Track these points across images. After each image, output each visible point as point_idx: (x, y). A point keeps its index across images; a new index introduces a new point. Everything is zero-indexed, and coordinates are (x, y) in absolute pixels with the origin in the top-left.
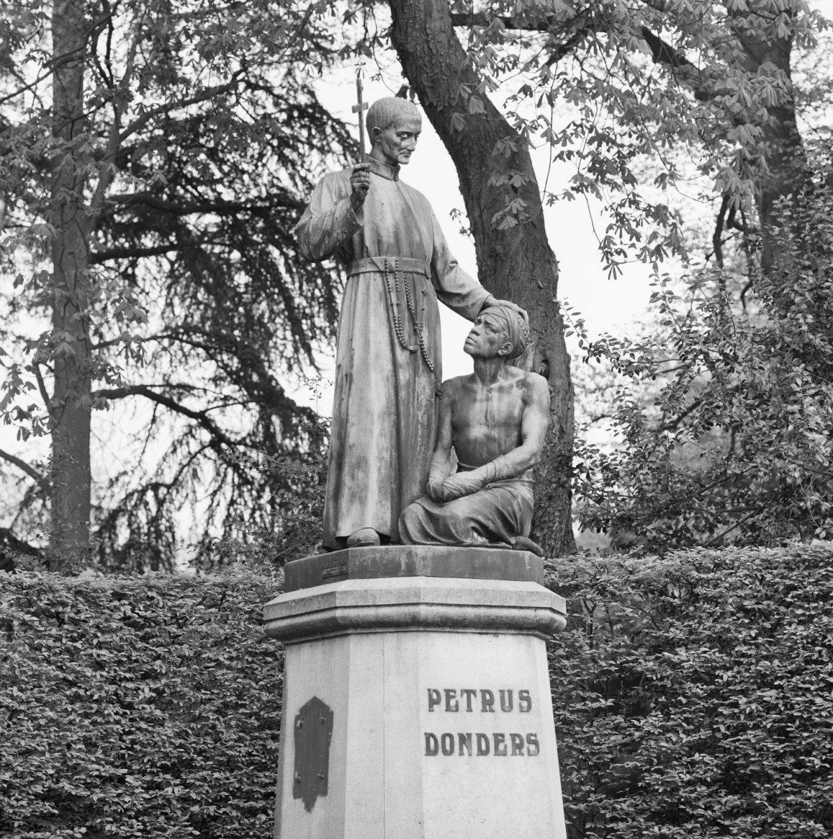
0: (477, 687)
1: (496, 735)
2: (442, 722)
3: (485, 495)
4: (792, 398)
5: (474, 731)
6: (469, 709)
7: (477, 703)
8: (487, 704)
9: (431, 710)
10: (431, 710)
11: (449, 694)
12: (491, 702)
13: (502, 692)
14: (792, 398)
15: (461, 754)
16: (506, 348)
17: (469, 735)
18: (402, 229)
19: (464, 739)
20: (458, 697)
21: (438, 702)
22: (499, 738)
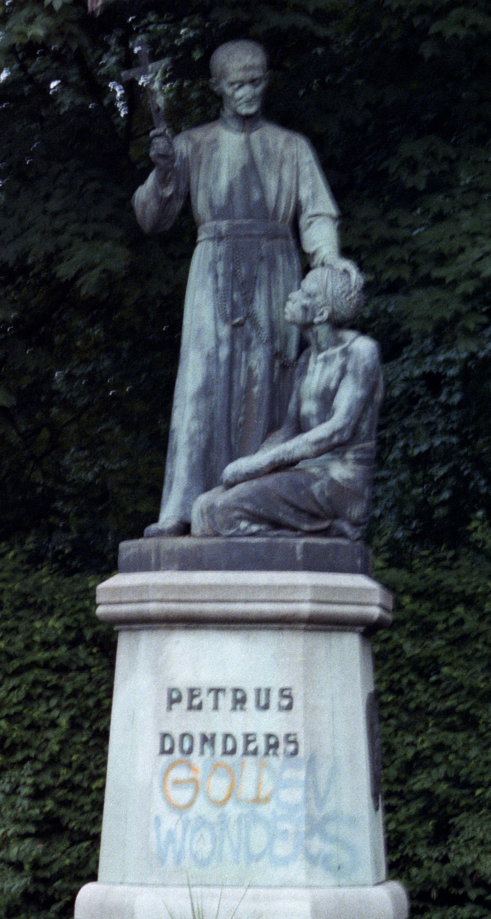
0: (229, 685)
1: (247, 736)
2: (180, 721)
3: (255, 483)
4: (334, 274)
5: (220, 730)
6: (216, 707)
7: (226, 701)
8: (240, 701)
9: (170, 709)
10: (170, 709)
11: (193, 693)
12: (243, 700)
13: (258, 691)
14: (334, 274)
15: (202, 753)
16: (346, 272)
17: (213, 736)
18: (238, 188)
19: (208, 740)
20: (203, 696)
21: (179, 700)
22: (248, 739)
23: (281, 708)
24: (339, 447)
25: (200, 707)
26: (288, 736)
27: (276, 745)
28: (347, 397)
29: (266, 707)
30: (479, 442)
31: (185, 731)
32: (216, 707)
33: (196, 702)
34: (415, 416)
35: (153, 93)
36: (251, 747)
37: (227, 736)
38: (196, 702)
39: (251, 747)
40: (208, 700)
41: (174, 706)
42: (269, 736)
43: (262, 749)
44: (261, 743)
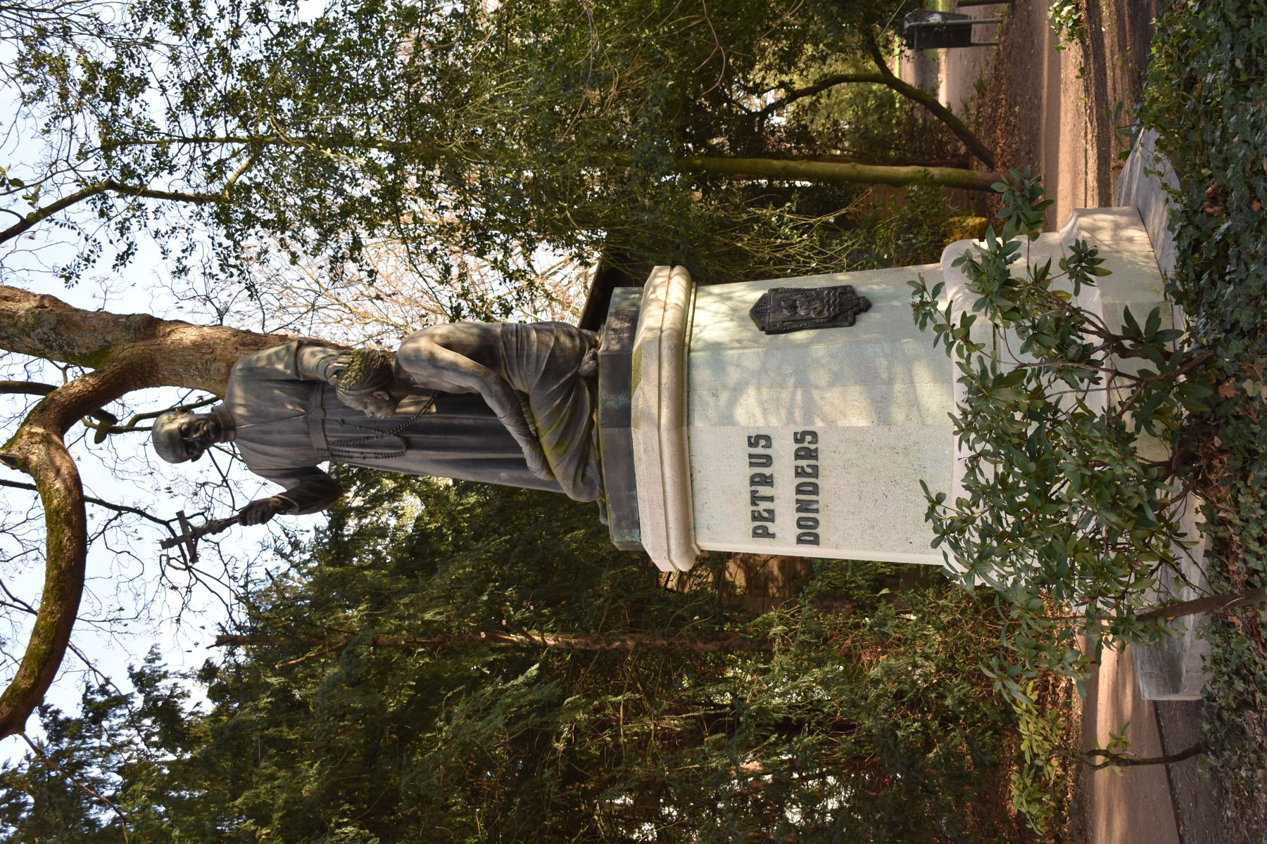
1: (798, 474)
6: (771, 499)
7: (764, 491)
8: (767, 481)
9: (773, 536)
10: (773, 536)
11: (756, 517)
13: (751, 464)
22: (799, 473)
23: (769, 446)
24: (1108, 185)
25: (771, 512)
26: (797, 441)
28: (585, 232)
30: (396, 348)
32: (771, 499)
35: (861, 47)
37: (798, 491)
38: (765, 515)
40: (763, 505)
42: (797, 457)
43: (812, 462)
44: (803, 463)
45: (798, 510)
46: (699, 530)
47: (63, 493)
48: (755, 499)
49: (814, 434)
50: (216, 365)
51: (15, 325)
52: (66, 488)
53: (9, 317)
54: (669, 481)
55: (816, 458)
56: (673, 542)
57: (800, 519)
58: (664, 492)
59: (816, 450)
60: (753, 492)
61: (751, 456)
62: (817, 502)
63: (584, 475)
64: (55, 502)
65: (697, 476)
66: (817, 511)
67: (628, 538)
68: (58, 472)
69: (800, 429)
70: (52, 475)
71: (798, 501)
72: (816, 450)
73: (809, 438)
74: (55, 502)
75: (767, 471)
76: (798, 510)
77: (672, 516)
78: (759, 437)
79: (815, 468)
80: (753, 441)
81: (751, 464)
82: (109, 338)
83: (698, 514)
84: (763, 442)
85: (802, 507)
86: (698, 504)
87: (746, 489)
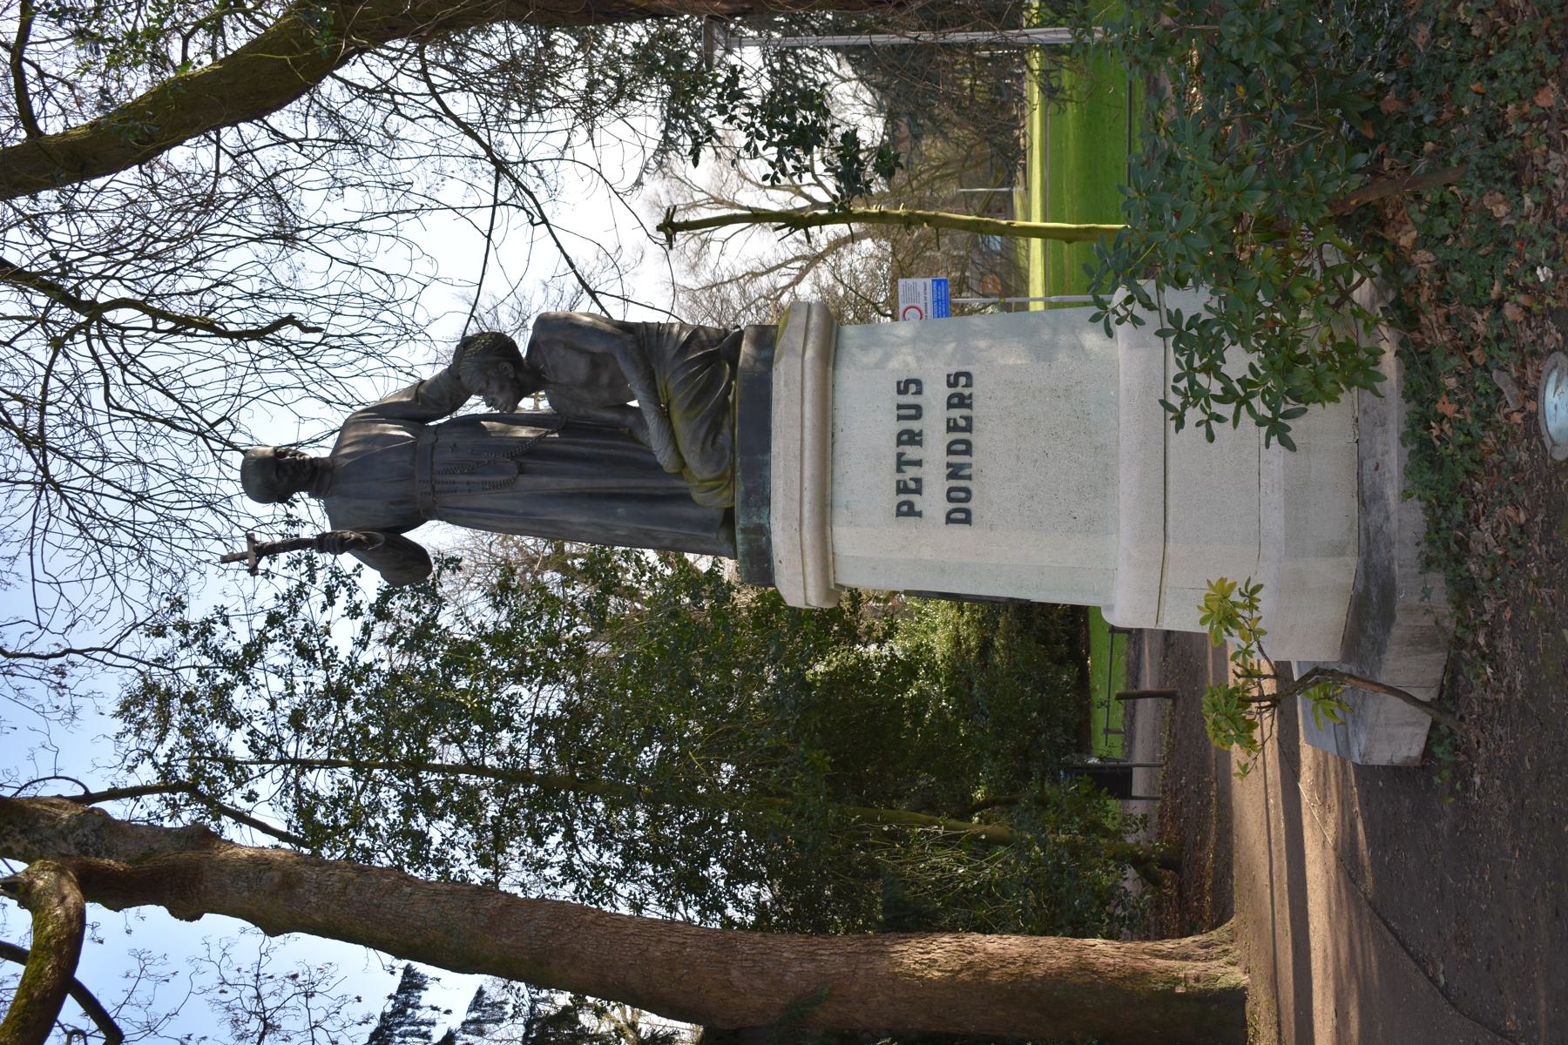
1: (949, 429)
2: (933, 500)
6: (919, 463)
7: (911, 452)
9: (919, 514)
10: (919, 514)
11: (902, 489)
13: (900, 418)
17: (949, 465)
21: (911, 505)
22: (952, 427)
23: (919, 392)
25: (918, 481)
26: (950, 385)
27: (961, 396)
29: (918, 408)
31: (925, 412)
32: (919, 463)
33: (912, 485)
34: (1383, 230)
36: (962, 423)
37: (950, 452)
38: (912, 485)
39: (962, 423)
40: (911, 472)
41: (917, 508)
42: (950, 406)
43: (965, 412)
44: (956, 413)
45: (950, 476)
46: (837, 511)
47: (62, 919)
48: (901, 463)
49: (968, 375)
50: (271, 874)
51: (54, 827)
52: (67, 916)
53: (50, 818)
54: (808, 424)
55: (970, 406)
56: (807, 507)
57: (950, 490)
58: (802, 440)
59: (970, 396)
60: (900, 455)
61: (899, 407)
62: (970, 465)
63: (714, 443)
64: (50, 928)
65: (839, 435)
66: (969, 477)
67: (755, 519)
68: (63, 899)
69: (953, 370)
70: (55, 900)
71: (949, 465)
72: (970, 396)
73: (963, 380)
74: (50, 928)
75: (914, 426)
76: (950, 476)
77: (808, 472)
78: (908, 382)
79: (968, 419)
80: (903, 387)
81: (900, 418)
82: (156, 846)
83: (836, 487)
84: (913, 388)
85: (955, 472)
86: (837, 475)
87: (890, 450)
